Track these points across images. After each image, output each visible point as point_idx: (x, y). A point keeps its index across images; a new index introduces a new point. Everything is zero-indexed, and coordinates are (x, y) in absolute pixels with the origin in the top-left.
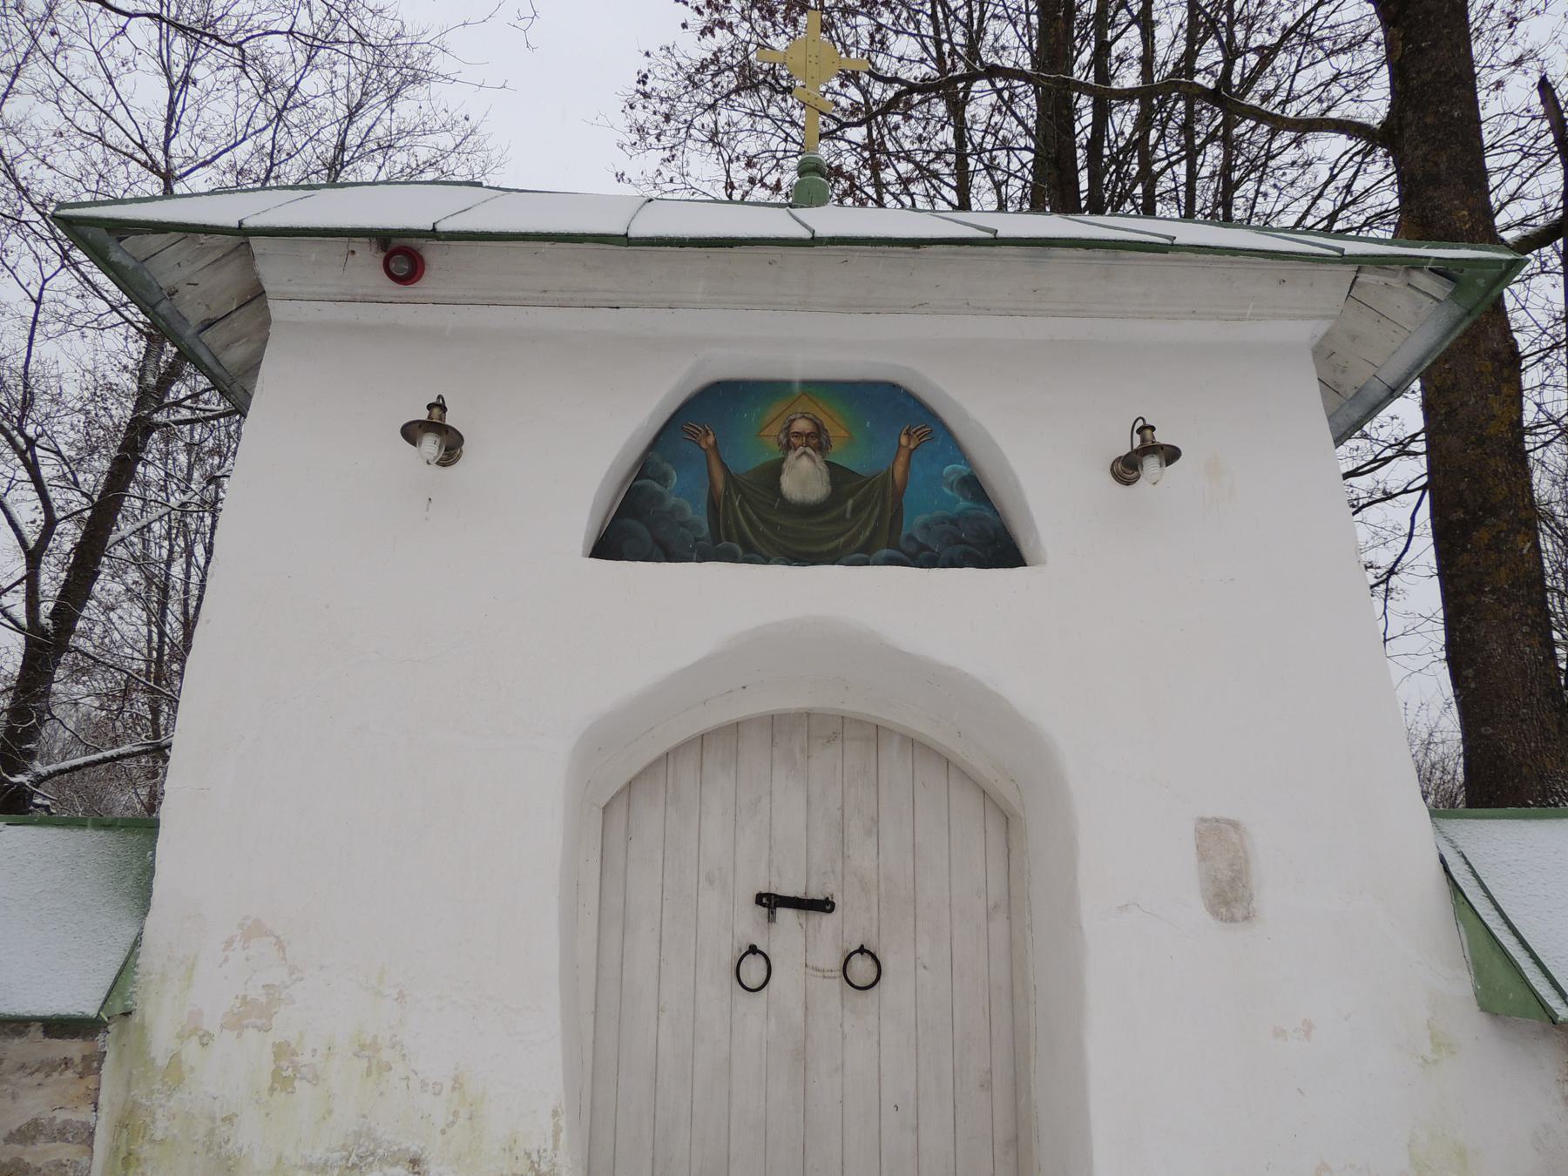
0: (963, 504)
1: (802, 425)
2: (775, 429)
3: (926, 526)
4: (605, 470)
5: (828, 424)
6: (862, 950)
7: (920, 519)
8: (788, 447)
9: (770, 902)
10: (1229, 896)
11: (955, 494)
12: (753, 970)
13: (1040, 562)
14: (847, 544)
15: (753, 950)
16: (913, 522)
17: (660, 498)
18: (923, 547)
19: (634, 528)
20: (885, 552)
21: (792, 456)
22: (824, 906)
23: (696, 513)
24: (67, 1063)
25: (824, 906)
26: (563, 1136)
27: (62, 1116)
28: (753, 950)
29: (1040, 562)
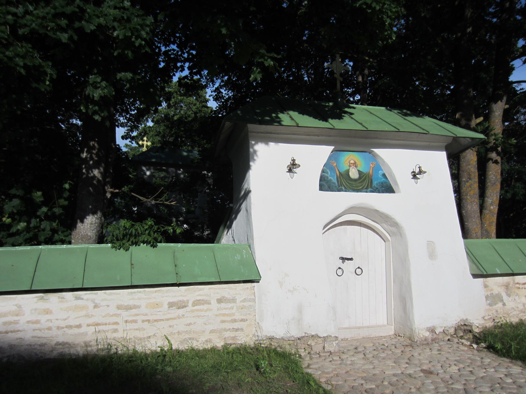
0: (383, 179)
1: (352, 162)
2: (347, 162)
3: (377, 184)
4: (395, 174)
5: (357, 161)
6: (359, 268)
7: (376, 182)
8: (350, 166)
9: (343, 259)
10: (432, 255)
11: (382, 177)
12: (340, 272)
13: (399, 192)
14: (362, 188)
15: (340, 268)
16: (375, 183)
17: (327, 177)
18: (377, 188)
19: (325, 185)
20: (370, 189)
21: (351, 168)
22: (351, 259)
23: (334, 180)
24: (248, 288)
25: (351, 259)
26: (38, 339)
27: (249, 297)
28: (340, 268)
29: (399, 192)
